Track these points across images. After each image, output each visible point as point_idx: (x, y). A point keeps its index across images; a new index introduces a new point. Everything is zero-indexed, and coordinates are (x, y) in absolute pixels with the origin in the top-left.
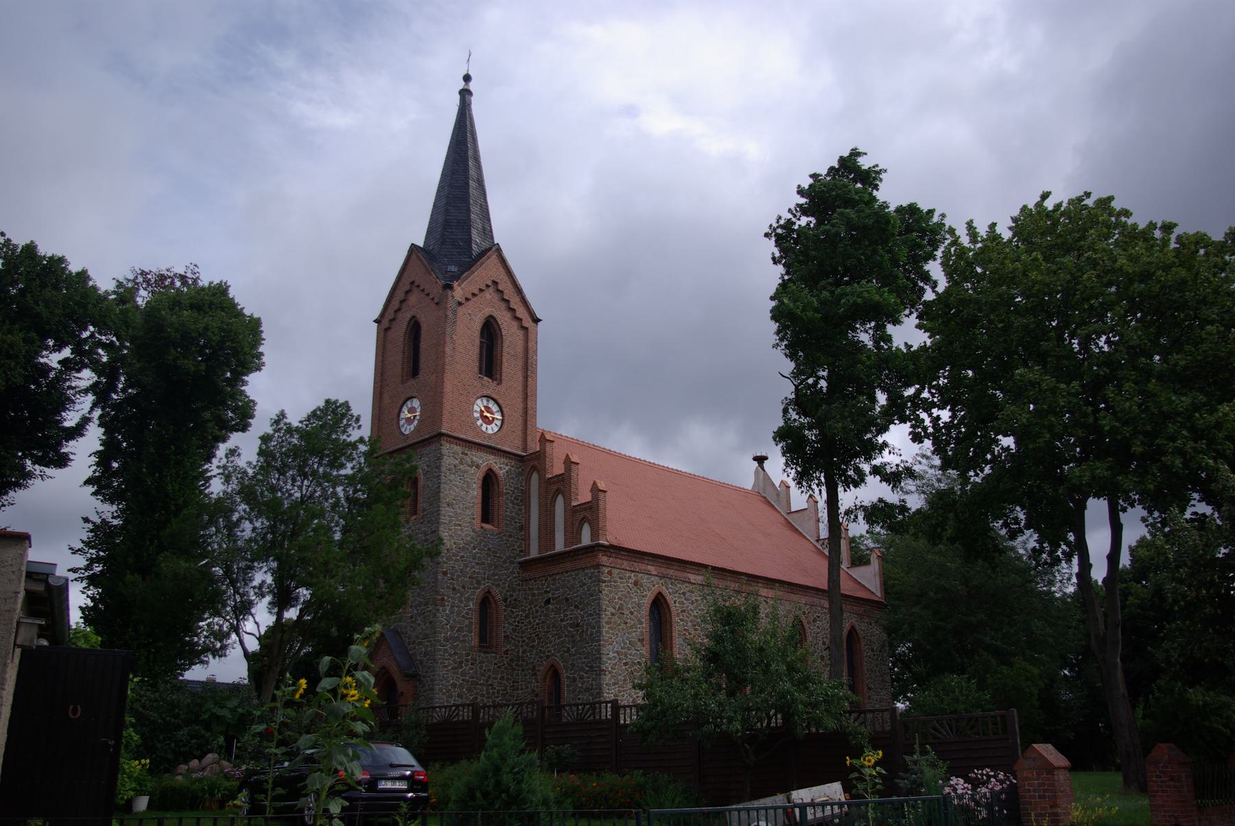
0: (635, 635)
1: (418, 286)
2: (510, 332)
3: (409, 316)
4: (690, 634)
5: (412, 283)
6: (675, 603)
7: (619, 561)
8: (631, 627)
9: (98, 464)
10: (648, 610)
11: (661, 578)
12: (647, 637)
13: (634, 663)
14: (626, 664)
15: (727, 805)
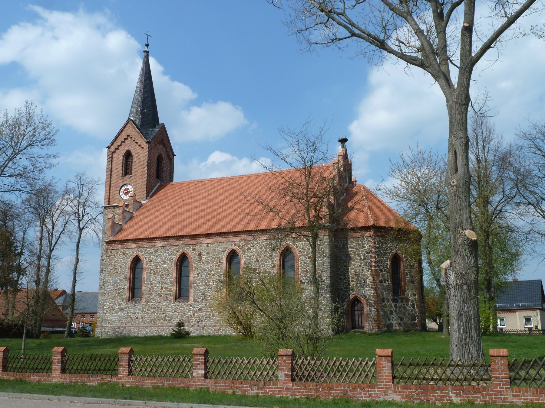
0: (122, 276)
1: (131, 138)
2: (166, 160)
3: (126, 149)
4: (154, 271)
5: (128, 136)
6: (146, 258)
7: (116, 246)
8: (120, 273)
9: (172, 334)
10: (130, 264)
11: (138, 248)
12: (128, 277)
13: (121, 289)
14: (116, 290)
15: (56, 327)
